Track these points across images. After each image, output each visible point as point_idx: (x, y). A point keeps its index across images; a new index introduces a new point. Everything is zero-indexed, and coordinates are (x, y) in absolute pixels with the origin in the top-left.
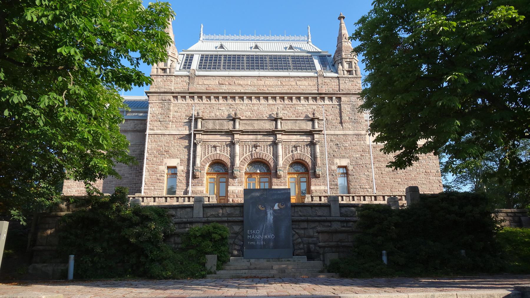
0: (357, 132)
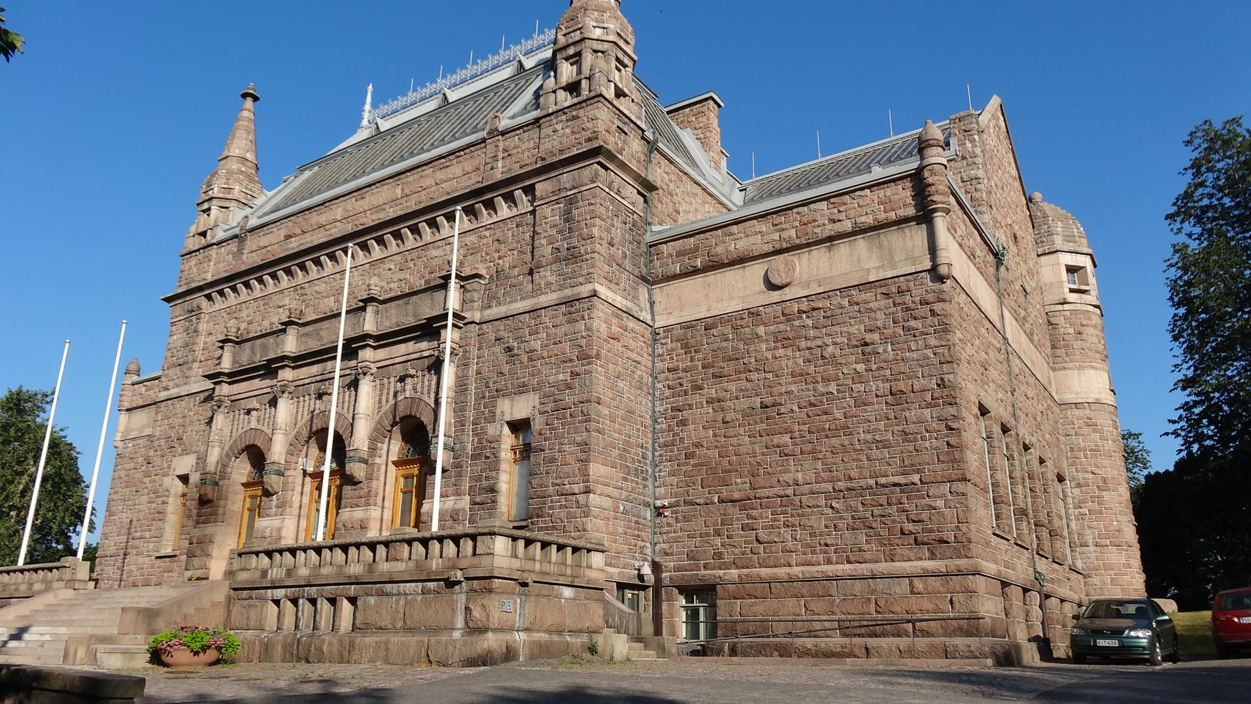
0: (570, 293)
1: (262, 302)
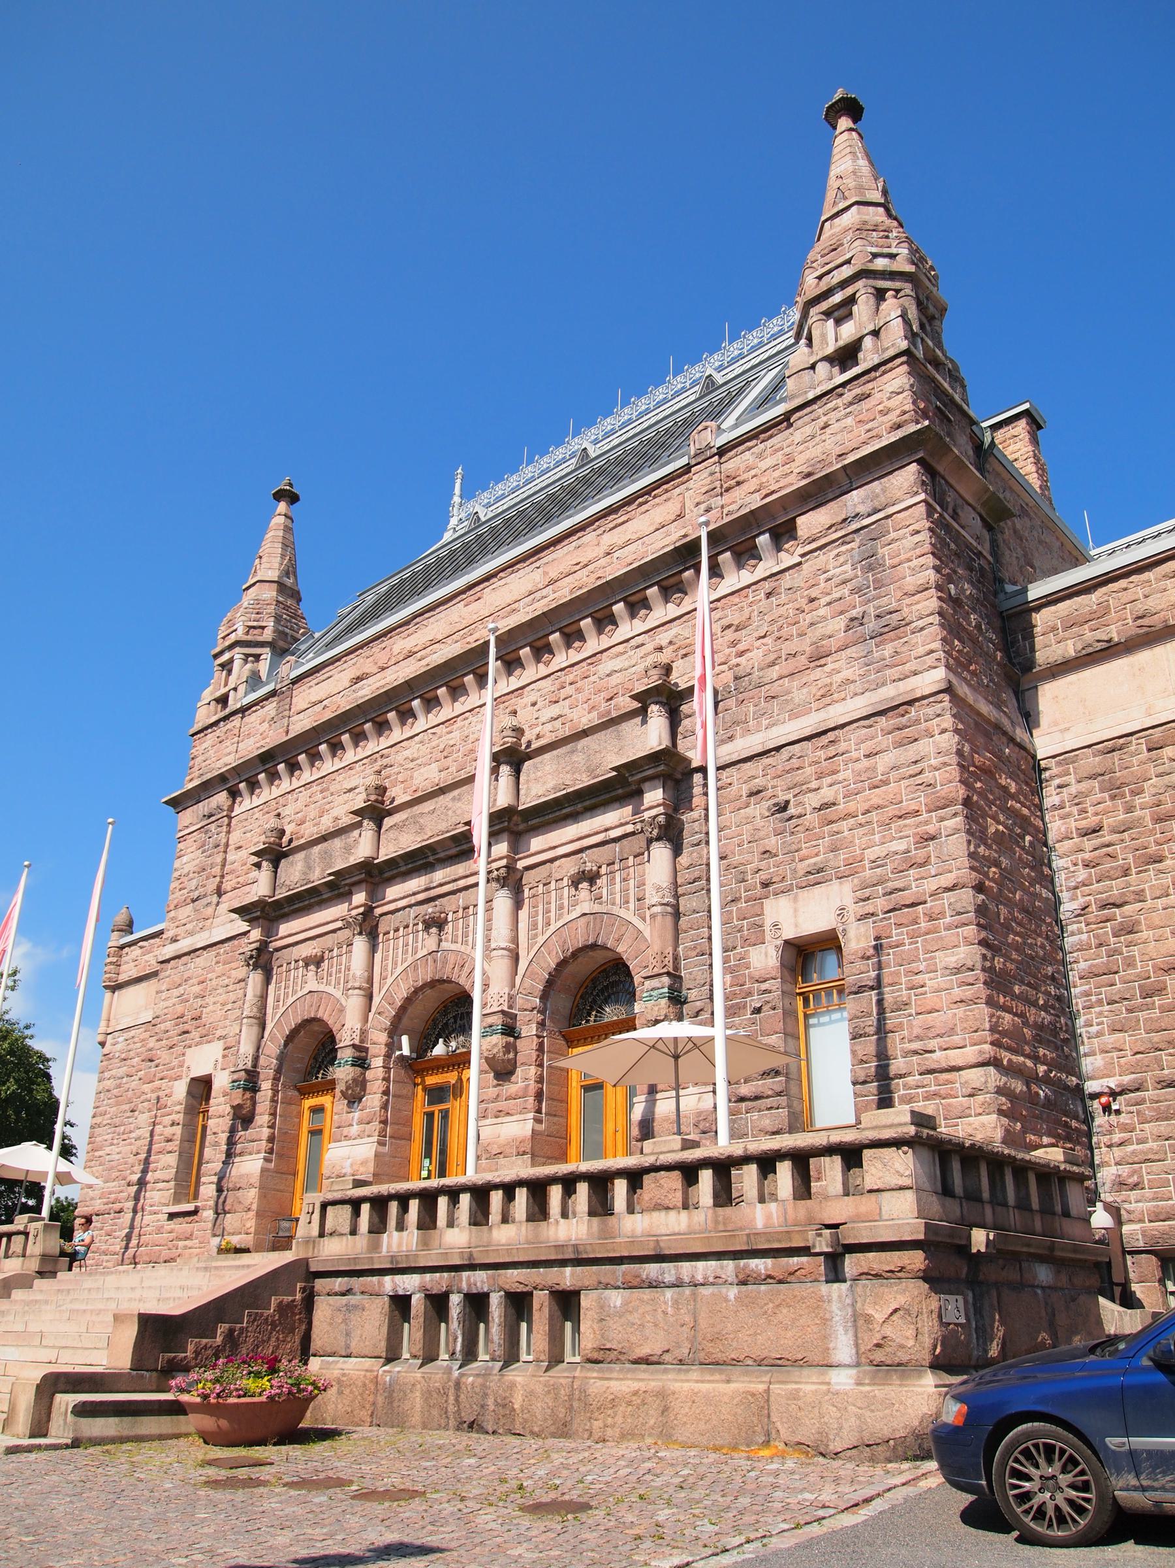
1: (319, 788)
